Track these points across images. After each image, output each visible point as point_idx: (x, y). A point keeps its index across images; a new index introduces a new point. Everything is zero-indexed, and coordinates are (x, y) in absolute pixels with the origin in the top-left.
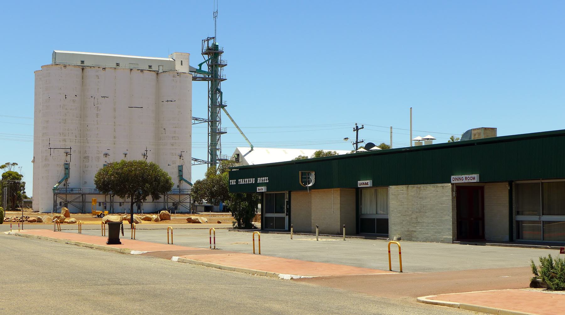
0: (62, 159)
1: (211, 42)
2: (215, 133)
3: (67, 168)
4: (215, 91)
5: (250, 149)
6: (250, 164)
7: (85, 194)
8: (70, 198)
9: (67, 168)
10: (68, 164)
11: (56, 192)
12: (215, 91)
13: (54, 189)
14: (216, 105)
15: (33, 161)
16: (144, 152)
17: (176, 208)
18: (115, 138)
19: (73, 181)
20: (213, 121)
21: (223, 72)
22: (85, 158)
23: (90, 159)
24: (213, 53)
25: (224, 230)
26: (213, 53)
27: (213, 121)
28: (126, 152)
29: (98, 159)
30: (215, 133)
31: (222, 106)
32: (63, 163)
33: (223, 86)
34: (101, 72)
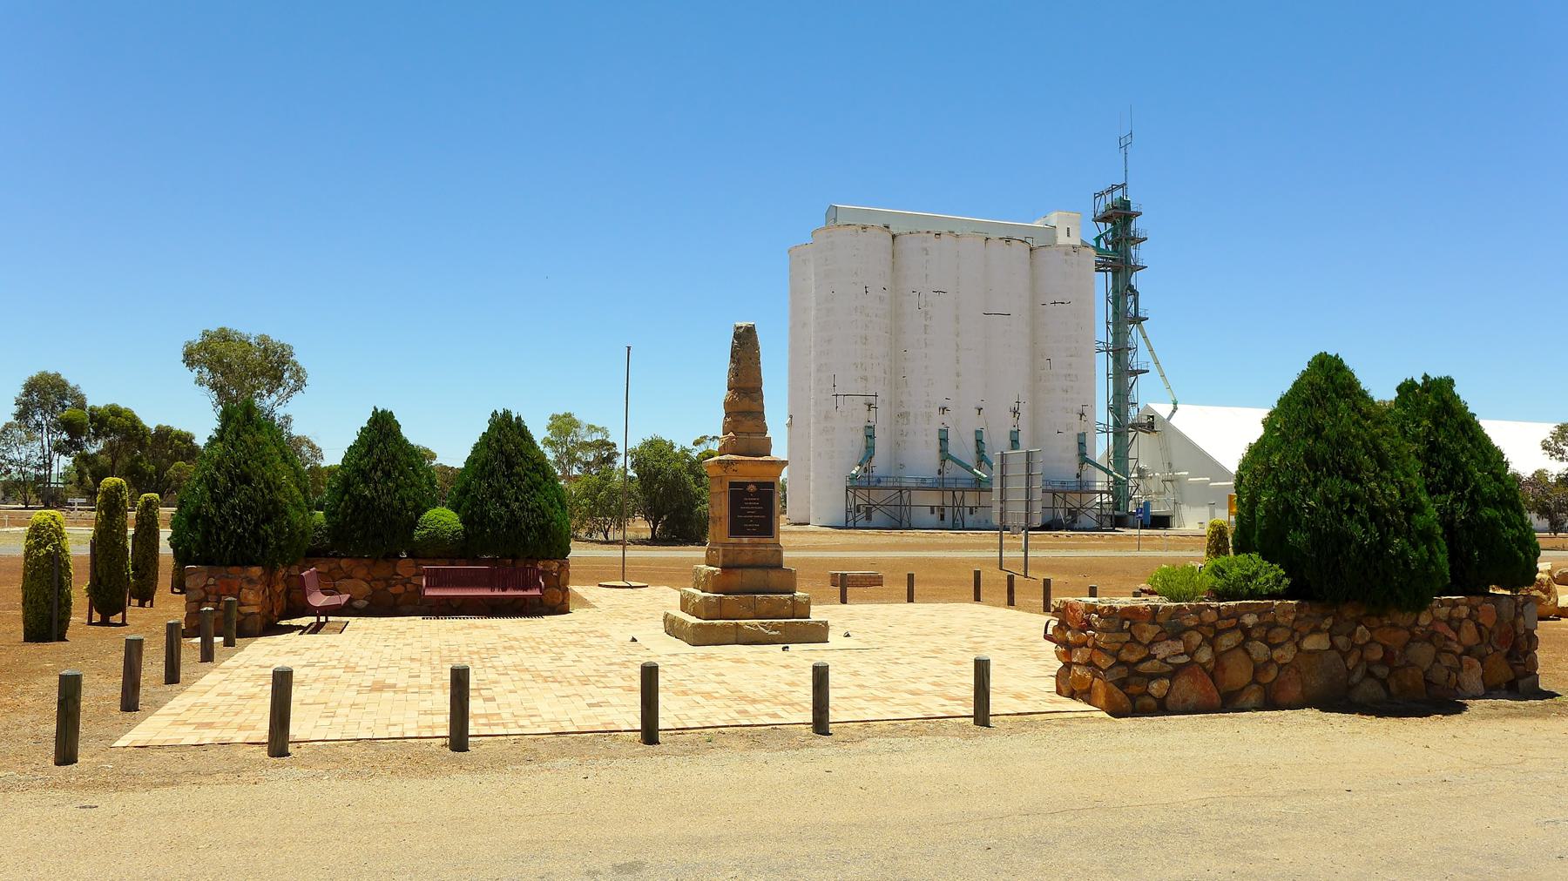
0: (861, 416)
1: (1118, 194)
2: (1123, 373)
3: (870, 435)
4: (1123, 293)
5: (1171, 407)
6: (460, 464)
7: (909, 489)
8: (877, 497)
9: (870, 435)
10: (872, 428)
11: (854, 485)
12: (1123, 293)
13: (853, 478)
14: (1125, 316)
15: (790, 425)
16: (1013, 405)
17: (1074, 521)
18: (958, 375)
19: (880, 464)
20: (1119, 351)
21: (1140, 254)
22: (901, 415)
23: (911, 418)
24: (1119, 217)
25: (256, 747)
26: (1119, 217)
27: (1119, 351)
28: (981, 405)
29: (929, 416)
30: (1123, 373)
31: (1137, 320)
32: (863, 424)
33: (1137, 280)
34: (932, 242)
